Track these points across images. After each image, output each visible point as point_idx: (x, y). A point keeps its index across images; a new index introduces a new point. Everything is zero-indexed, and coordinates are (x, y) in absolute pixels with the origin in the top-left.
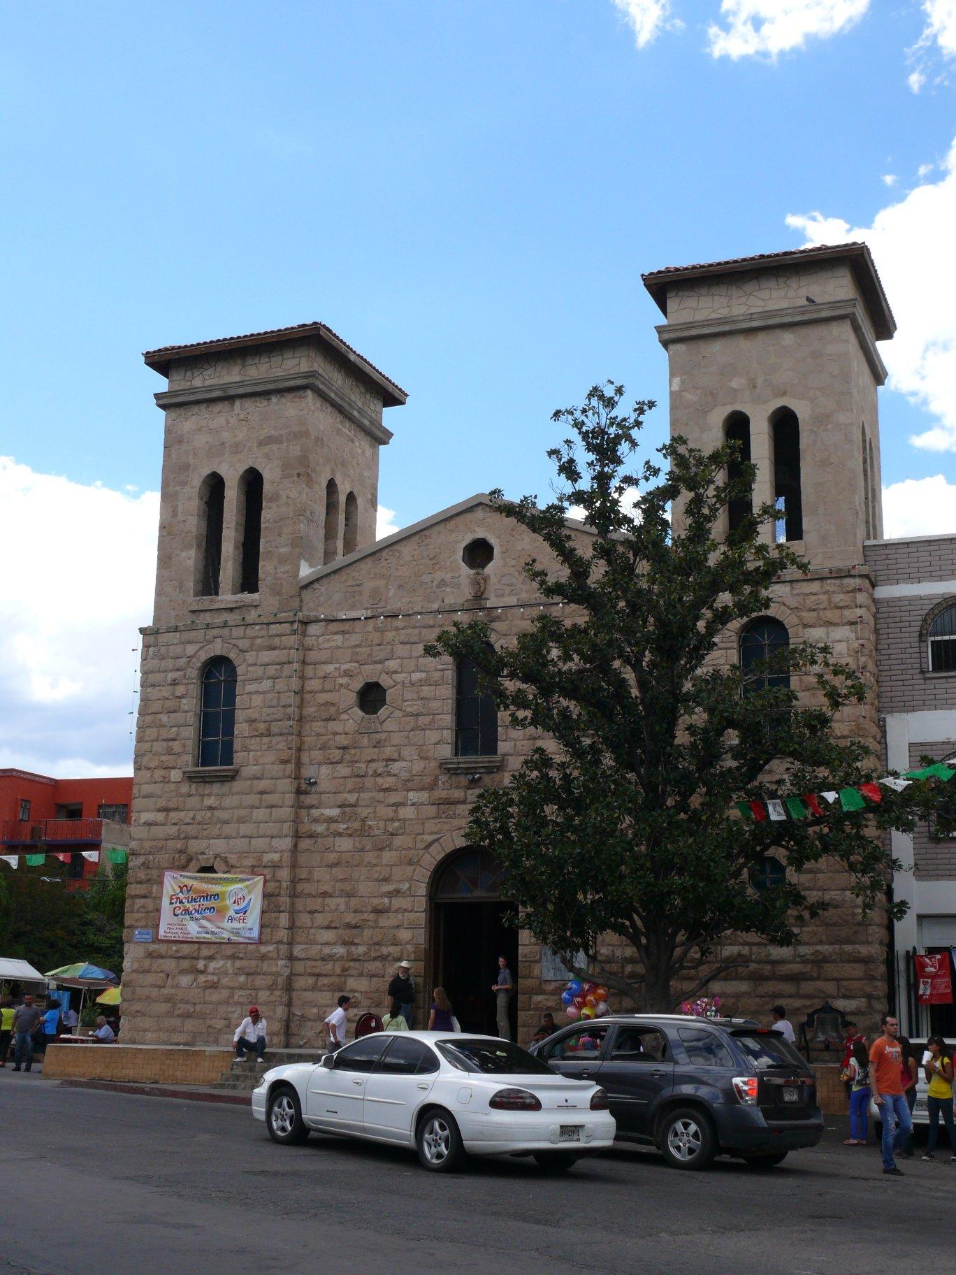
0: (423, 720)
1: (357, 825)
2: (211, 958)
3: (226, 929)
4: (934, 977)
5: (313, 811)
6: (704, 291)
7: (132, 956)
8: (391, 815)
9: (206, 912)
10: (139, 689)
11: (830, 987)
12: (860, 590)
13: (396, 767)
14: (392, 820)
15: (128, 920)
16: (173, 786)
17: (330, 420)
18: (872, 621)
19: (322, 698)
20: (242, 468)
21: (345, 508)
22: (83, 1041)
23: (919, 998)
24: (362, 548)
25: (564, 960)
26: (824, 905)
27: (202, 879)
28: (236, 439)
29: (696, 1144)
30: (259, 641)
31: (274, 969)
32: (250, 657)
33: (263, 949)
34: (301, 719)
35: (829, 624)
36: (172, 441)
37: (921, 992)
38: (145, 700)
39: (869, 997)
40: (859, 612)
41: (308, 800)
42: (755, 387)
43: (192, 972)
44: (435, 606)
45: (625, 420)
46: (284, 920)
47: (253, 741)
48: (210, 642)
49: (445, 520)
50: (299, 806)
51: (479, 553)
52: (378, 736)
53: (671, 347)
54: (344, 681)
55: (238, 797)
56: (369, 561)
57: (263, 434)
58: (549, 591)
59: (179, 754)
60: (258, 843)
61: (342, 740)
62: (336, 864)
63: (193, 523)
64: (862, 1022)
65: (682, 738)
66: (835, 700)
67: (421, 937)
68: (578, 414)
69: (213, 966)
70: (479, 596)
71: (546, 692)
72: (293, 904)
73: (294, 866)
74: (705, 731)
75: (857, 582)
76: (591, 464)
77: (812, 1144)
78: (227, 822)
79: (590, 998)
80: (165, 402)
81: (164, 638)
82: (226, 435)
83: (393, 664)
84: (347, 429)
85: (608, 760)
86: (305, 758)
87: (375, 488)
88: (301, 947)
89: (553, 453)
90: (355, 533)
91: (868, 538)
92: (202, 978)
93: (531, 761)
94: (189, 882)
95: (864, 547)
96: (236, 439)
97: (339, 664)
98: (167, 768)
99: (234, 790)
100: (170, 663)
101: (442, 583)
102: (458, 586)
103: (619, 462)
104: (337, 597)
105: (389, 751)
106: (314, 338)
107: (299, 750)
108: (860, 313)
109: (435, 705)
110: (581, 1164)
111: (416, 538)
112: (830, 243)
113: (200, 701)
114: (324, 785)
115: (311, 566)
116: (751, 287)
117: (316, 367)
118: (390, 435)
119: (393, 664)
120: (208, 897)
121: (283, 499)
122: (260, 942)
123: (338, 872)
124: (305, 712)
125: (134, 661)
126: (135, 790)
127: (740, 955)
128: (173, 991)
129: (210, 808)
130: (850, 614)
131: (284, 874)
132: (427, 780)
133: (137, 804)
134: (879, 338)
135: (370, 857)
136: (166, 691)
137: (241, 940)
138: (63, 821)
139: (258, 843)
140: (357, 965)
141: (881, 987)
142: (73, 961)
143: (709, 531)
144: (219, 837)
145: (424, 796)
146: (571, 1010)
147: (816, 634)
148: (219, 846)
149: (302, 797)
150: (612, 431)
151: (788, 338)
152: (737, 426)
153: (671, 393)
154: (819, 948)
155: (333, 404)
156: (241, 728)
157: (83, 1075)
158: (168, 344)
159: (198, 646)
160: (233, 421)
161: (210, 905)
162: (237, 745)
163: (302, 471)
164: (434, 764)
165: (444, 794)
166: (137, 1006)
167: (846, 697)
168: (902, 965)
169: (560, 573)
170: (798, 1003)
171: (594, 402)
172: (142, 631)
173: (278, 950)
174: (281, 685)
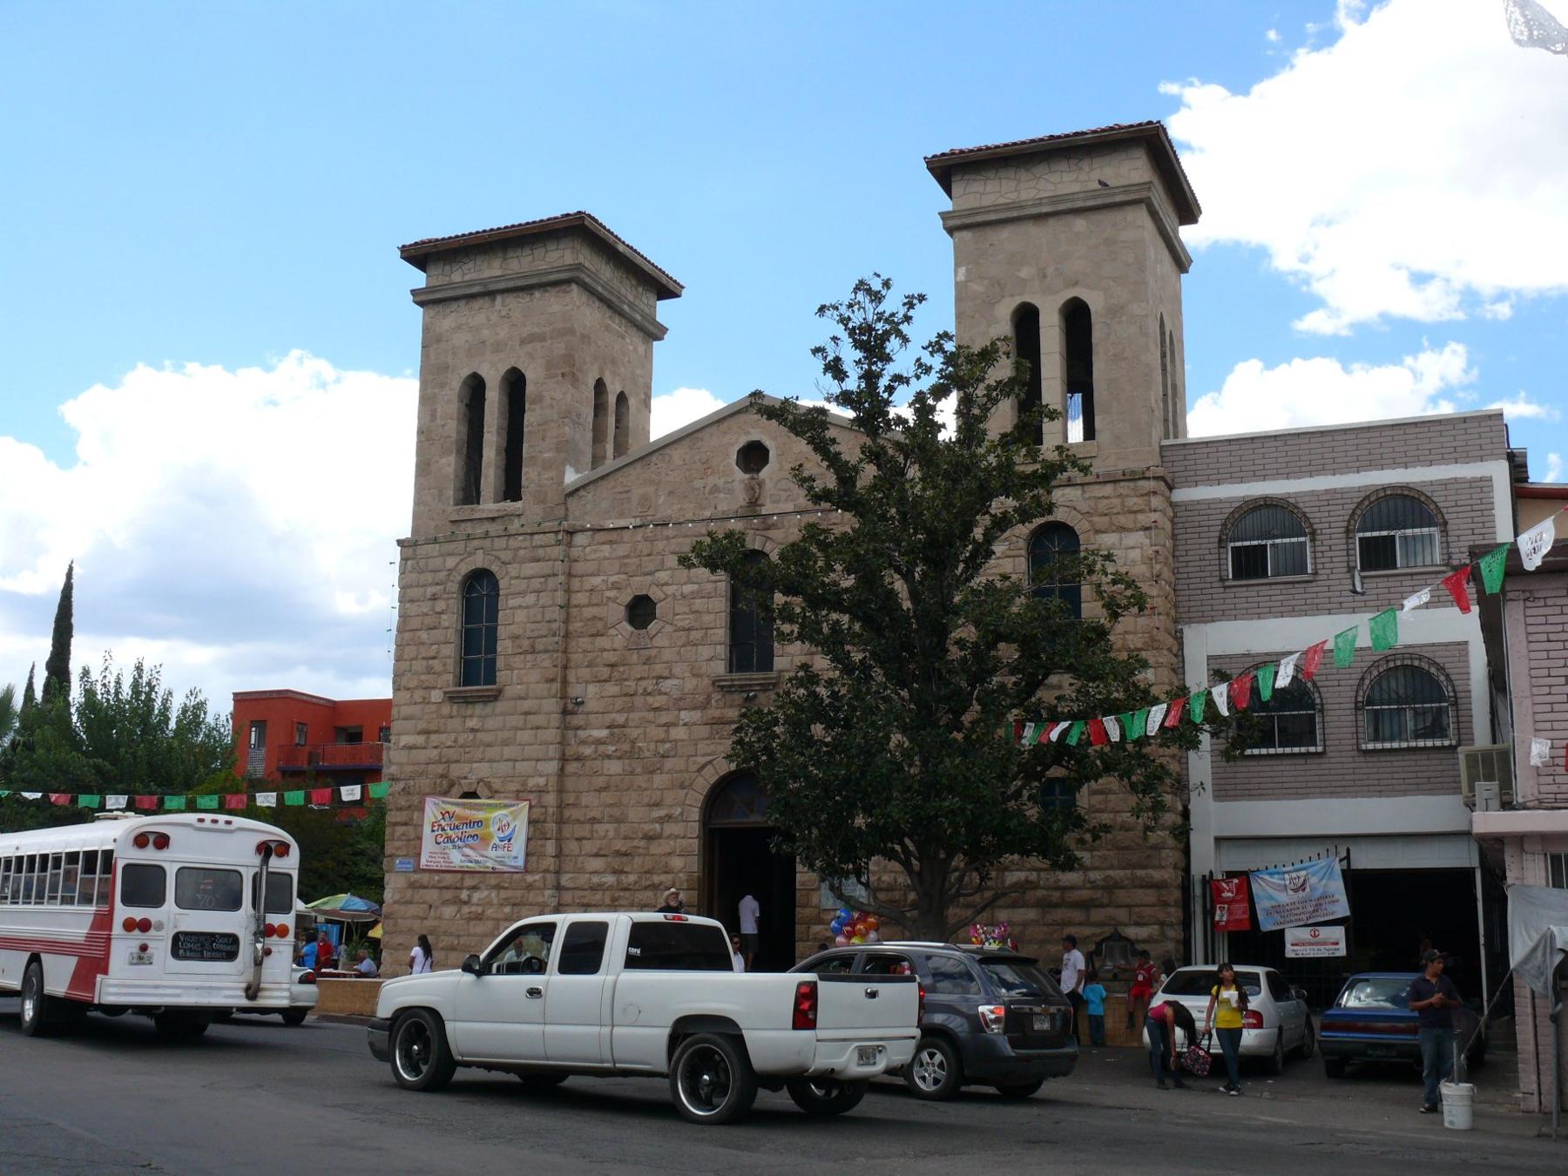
0: (695, 635)
1: (626, 747)
2: (475, 888)
3: (491, 857)
4: (1230, 902)
5: (580, 732)
6: (991, 174)
7: (394, 886)
8: (662, 735)
9: (462, 838)
10: (397, 604)
11: (1121, 914)
12: (1155, 493)
13: (667, 685)
14: (663, 741)
15: (388, 850)
16: (433, 708)
17: (598, 315)
18: (1168, 525)
19: (589, 612)
20: (504, 368)
21: (615, 410)
22: (344, 976)
23: (1215, 925)
24: (635, 451)
25: (832, 888)
26: (1107, 828)
27: (463, 805)
28: (496, 338)
29: (942, 1074)
30: (522, 552)
31: (540, 899)
32: (513, 570)
33: (529, 878)
34: (567, 635)
35: (1122, 529)
36: (431, 340)
37: (1217, 918)
38: (403, 616)
39: (1162, 924)
40: (1154, 516)
41: (576, 720)
42: (1045, 276)
43: (454, 903)
44: (707, 514)
45: (893, 315)
46: (550, 847)
47: (517, 658)
48: (470, 554)
49: (718, 421)
50: (565, 727)
51: (754, 456)
52: (647, 652)
53: (956, 234)
54: (612, 594)
55: (500, 718)
56: (638, 466)
57: (526, 331)
58: (817, 498)
59: (439, 674)
60: (523, 767)
61: (611, 657)
62: (605, 789)
63: (453, 428)
64: (1155, 951)
65: (955, 653)
66: (1114, 612)
67: (694, 864)
68: (843, 310)
69: (476, 896)
70: (754, 503)
71: (815, 603)
72: (560, 831)
73: (561, 790)
74: (976, 645)
75: (1152, 484)
76: (858, 362)
77: (1065, 1074)
78: (490, 745)
79: (860, 927)
80: (423, 298)
81: (423, 550)
82: (486, 333)
83: (663, 576)
84: (616, 325)
85: (878, 674)
86: (571, 677)
87: (649, 388)
88: (568, 876)
89: (817, 350)
90: (627, 435)
91: (1167, 437)
92: (466, 909)
93: (796, 678)
94: (451, 809)
95: (1161, 447)
96: (496, 338)
97: (606, 578)
98: (427, 688)
99: (498, 711)
100: (429, 578)
101: (715, 489)
102: (730, 491)
103: (887, 359)
104: (604, 505)
105: (659, 669)
106: (579, 229)
107: (565, 667)
108: (1159, 197)
109: (707, 619)
110: (869, 1105)
111: (687, 442)
112: (1125, 122)
113: (463, 616)
114: (591, 705)
115: (577, 471)
116: (1040, 170)
117: (581, 259)
118: (664, 330)
119: (663, 576)
120: (471, 823)
121: (548, 401)
122: (526, 871)
123: (607, 797)
124: (571, 628)
125: (392, 577)
126: (394, 711)
127: (1027, 881)
128: (436, 923)
129: (473, 730)
130: (1144, 519)
131: (550, 799)
132: (701, 698)
133: (396, 726)
134: (1182, 223)
135: (641, 781)
136: (425, 607)
137: (505, 869)
138: (343, 745)
139: (523, 767)
140: (627, 894)
141: (1175, 914)
142: (334, 891)
143: (984, 432)
144: (482, 760)
145: (696, 716)
146: (840, 939)
147: (1108, 540)
148: (483, 770)
149: (569, 717)
150: (880, 326)
151: (1080, 224)
152: (1026, 318)
153: (957, 284)
154: (1111, 873)
155: (601, 299)
156: (504, 646)
157: (342, 1011)
158: (425, 237)
159: (458, 559)
160: (494, 318)
161: (473, 832)
162: (500, 662)
163: (568, 370)
164: (706, 682)
165: (717, 713)
166: (399, 939)
167: (1126, 608)
168: (1198, 890)
169: (829, 481)
170: (1087, 931)
171: (860, 296)
172: (400, 542)
173: (544, 879)
174: (545, 599)
